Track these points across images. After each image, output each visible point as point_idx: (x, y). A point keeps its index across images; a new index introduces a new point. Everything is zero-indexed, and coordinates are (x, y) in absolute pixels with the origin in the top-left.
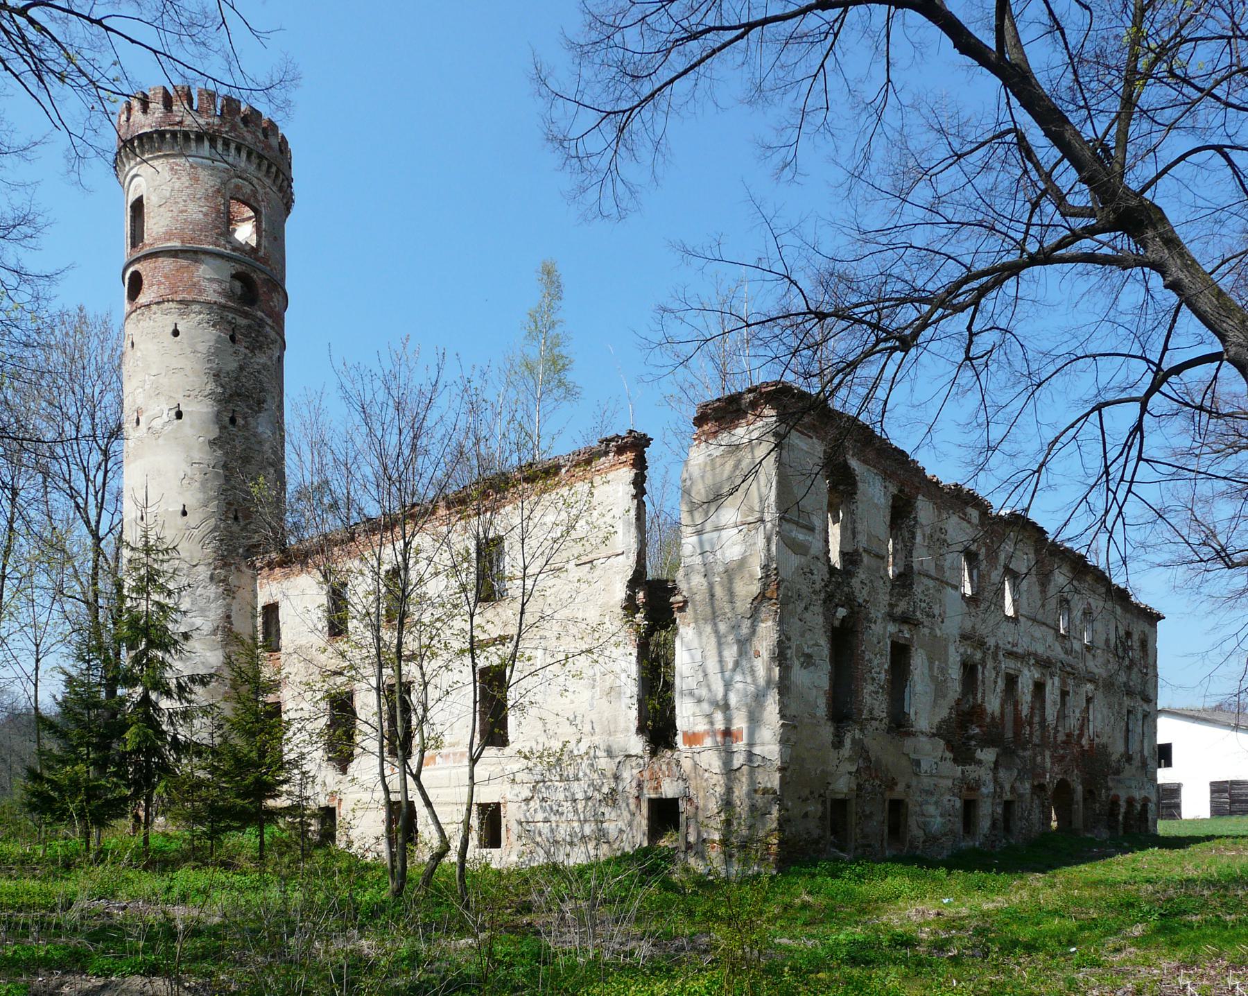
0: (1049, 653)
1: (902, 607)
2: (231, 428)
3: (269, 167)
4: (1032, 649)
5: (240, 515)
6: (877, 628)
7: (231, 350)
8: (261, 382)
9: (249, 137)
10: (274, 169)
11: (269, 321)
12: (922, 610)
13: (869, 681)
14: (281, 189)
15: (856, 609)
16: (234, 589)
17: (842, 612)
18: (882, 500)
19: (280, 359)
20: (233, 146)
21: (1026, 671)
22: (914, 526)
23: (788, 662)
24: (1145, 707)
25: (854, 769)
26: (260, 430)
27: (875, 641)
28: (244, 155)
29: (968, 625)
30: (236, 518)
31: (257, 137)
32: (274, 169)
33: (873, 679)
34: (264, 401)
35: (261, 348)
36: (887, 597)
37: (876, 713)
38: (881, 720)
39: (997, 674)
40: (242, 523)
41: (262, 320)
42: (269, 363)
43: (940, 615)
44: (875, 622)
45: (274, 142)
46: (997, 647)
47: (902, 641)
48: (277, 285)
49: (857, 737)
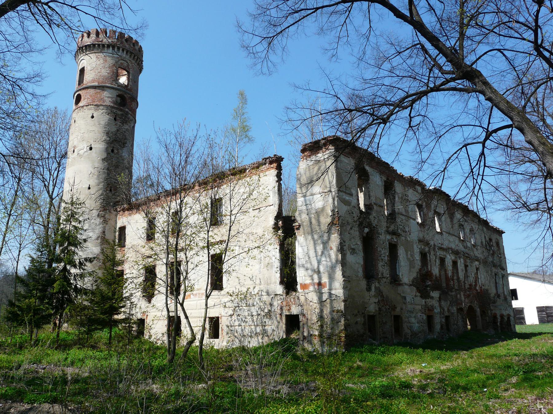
0: (457, 248)
1: (392, 228)
2: (112, 154)
3: (134, 56)
4: (450, 246)
5: (112, 189)
6: (382, 237)
7: (114, 123)
8: (125, 136)
9: (127, 46)
10: (136, 57)
11: (130, 113)
12: (401, 229)
13: (381, 260)
14: (138, 64)
15: (373, 229)
16: (108, 220)
17: (366, 230)
18: (380, 183)
19: (134, 127)
20: (121, 49)
21: (448, 256)
22: (394, 193)
23: (345, 252)
24: (502, 272)
25: (377, 301)
26: (123, 154)
27: (382, 243)
28: (125, 52)
29: (421, 236)
30: (111, 190)
31: (130, 46)
32: (136, 57)
33: (382, 259)
34: (126, 143)
35: (126, 123)
36: (386, 224)
37: (385, 275)
38: (387, 278)
39: (436, 257)
40: (113, 192)
41: (127, 112)
42: (129, 128)
43: (409, 231)
44: (381, 235)
45: (137, 48)
46: (434, 245)
47: (393, 243)
48: (134, 99)
49: (377, 286)
